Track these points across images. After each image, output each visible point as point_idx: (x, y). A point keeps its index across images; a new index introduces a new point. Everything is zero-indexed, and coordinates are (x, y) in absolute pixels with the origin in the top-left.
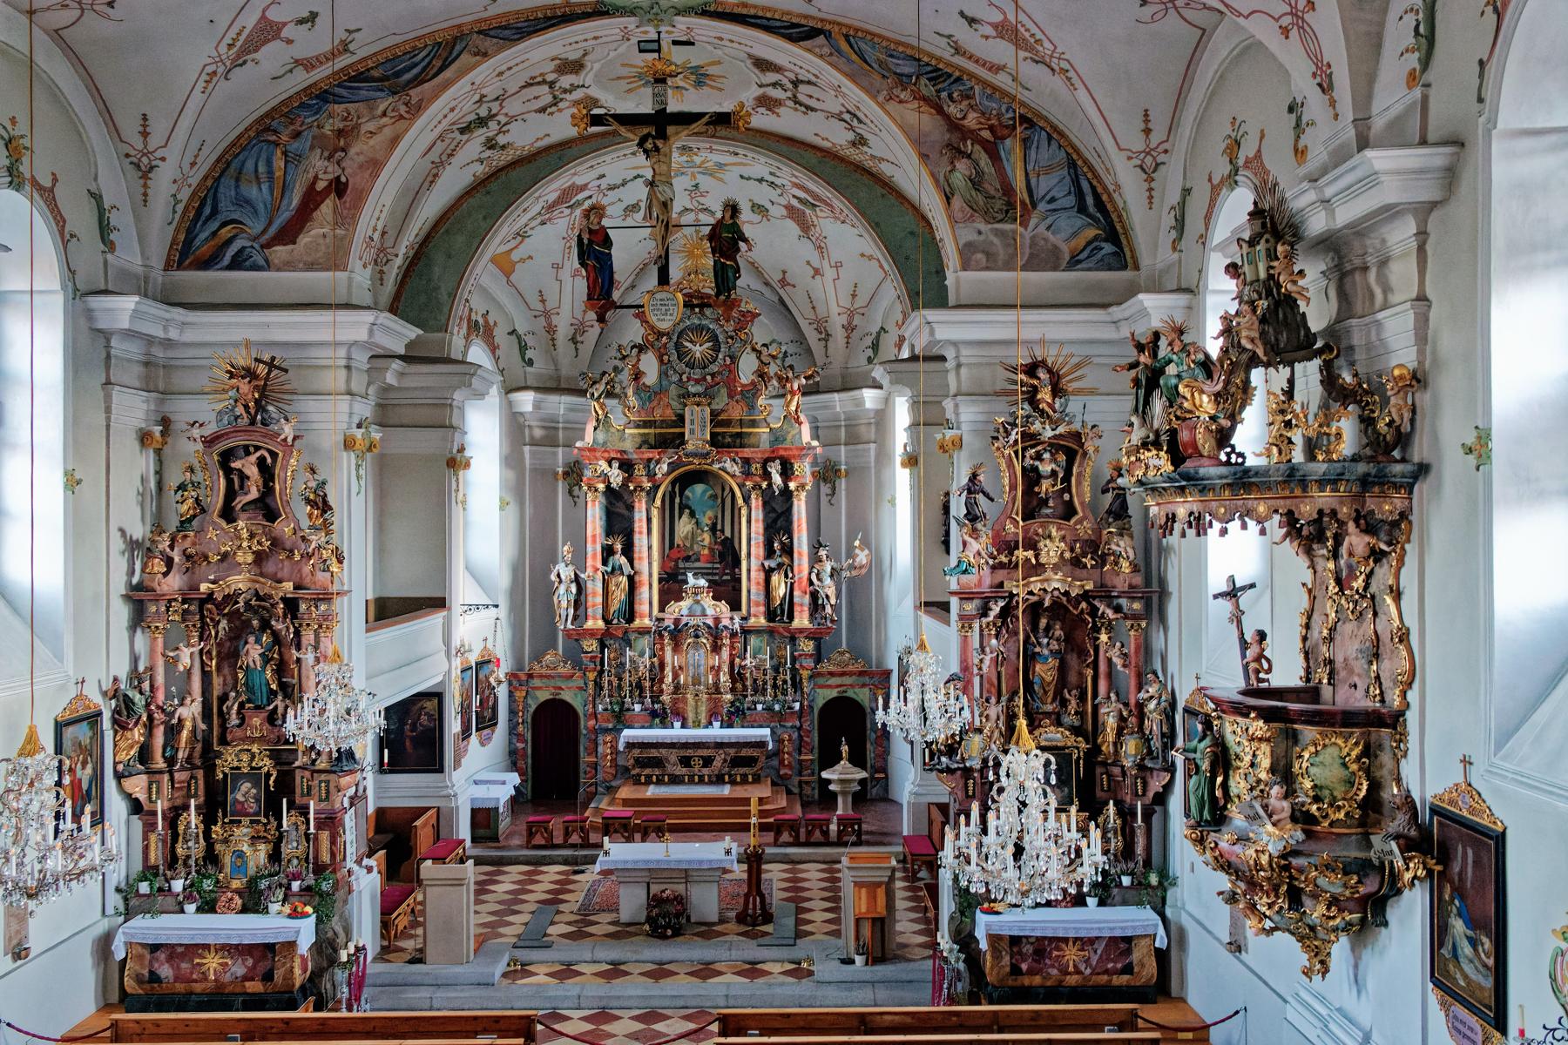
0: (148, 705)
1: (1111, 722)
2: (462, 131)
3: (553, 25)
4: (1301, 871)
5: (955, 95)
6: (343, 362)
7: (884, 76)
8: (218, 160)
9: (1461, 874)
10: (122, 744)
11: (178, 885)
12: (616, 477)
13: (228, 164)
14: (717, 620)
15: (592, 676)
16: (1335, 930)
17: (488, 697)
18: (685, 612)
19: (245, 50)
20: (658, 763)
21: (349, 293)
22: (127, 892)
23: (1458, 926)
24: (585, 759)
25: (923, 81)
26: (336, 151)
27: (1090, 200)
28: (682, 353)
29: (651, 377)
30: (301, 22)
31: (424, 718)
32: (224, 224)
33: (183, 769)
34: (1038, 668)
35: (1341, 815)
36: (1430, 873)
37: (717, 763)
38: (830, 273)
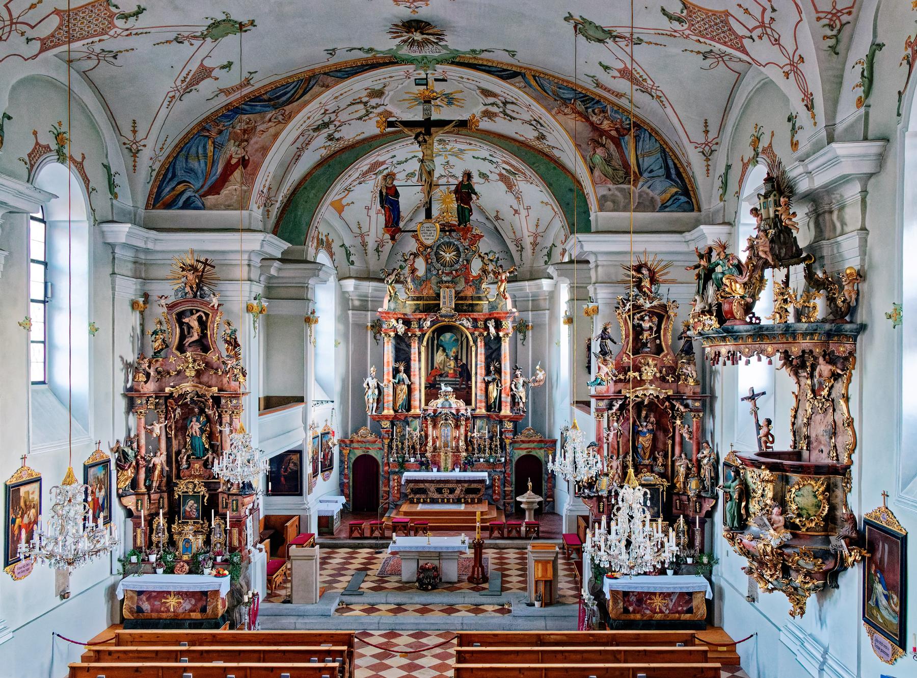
0: (136, 456)
1: (682, 470)
2: (315, 130)
4: (789, 556)
5: (596, 111)
7: (555, 100)
8: (176, 146)
9: (882, 559)
10: (122, 478)
11: (153, 558)
12: (401, 329)
14: (458, 410)
15: (386, 441)
16: (809, 590)
17: (328, 453)
18: (440, 406)
19: (191, 84)
20: (424, 491)
21: (250, 223)
22: (125, 561)
23: (879, 588)
24: (382, 488)
25: (578, 102)
27: (673, 171)
30: (223, 67)
31: (291, 465)
32: (179, 183)
33: (156, 492)
34: (640, 439)
35: (813, 525)
36: (863, 558)
37: (458, 492)
38: (523, 213)
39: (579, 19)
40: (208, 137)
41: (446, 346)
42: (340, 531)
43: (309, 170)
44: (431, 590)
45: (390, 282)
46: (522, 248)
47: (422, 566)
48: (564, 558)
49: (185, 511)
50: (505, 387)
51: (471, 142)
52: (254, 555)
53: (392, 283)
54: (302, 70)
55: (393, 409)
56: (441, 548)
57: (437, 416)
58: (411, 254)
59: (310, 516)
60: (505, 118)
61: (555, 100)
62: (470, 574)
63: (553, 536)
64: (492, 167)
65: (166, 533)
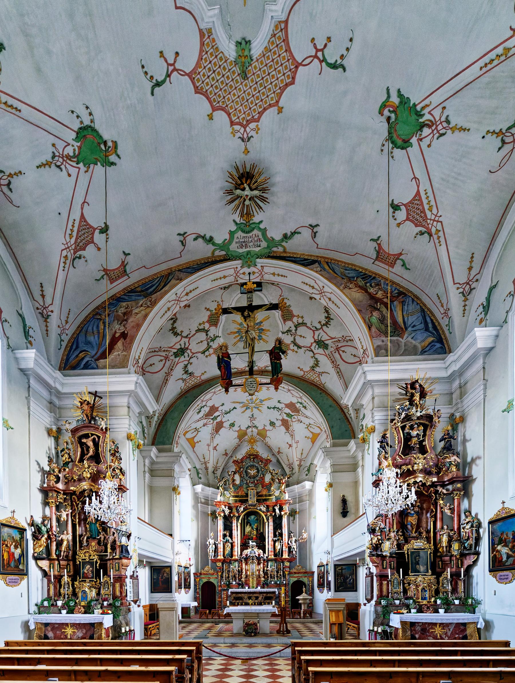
1: (445, 539)
3: (208, 266)
5: (373, 284)
6: (126, 404)
7: (343, 278)
8: (78, 327)
11: (60, 603)
12: (227, 511)
13: (82, 328)
14: (259, 555)
15: (220, 574)
18: (249, 553)
20: (241, 598)
24: (218, 599)
25: (359, 279)
26: (123, 321)
27: (430, 325)
29: (238, 482)
31: (165, 574)
33: (63, 560)
37: (260, 599)
38: (294, 445)
40: (100, 319)
41: (251, 523)
44: (254, 636)
46: (293, 469)
49: (84, 573)
52: (133, 607)
61: (343, 278)
65: (71, 588)
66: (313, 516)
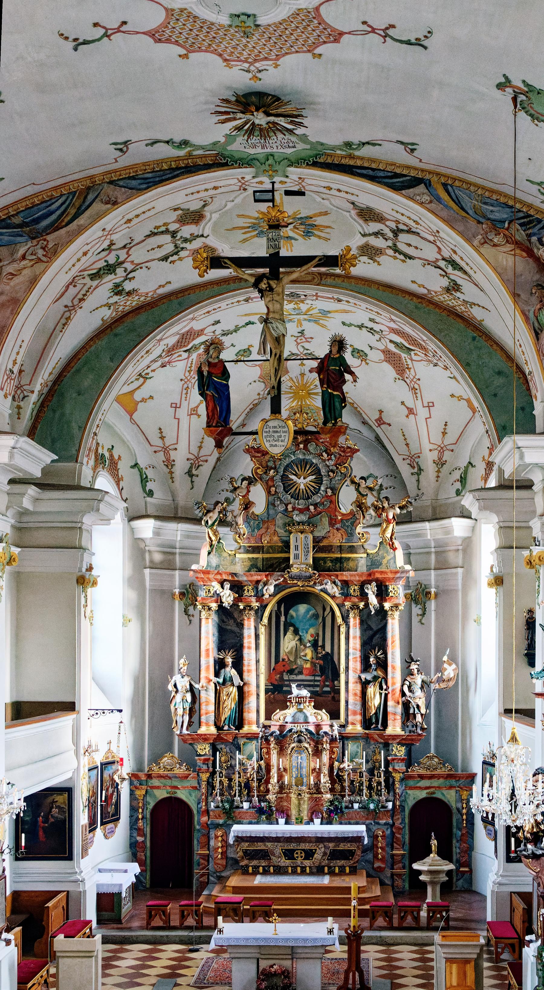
2: (93, 277)
12: (228, 597)
14: (318, 727)
15: (205, 777)
17: (112, 794)
18: (289, 719)
20: (265, 855)
24: (198, 851)
28: (288, 486)
29: (259, 508)
31: (55, 811)
38: (422, 413)
39: (521, 85)
41: (300, 626)
42: (132, 917)
43: (82, 344)
45: (210, 522)
46: (420, 469)
47: (264, 970)
48: (489, 960)
50: (393, 690)
51: (341, 297)
53: (213, 524)
54: (76, 177)
55: (216, 725)
56: (296, 940)
57: (284, 736)
58: (243, 480)
59: (85, 892)
60: (395, 258)
62: (341, 983)
63: (469, 925)
64: (372, 339)
66: (473, 615)
